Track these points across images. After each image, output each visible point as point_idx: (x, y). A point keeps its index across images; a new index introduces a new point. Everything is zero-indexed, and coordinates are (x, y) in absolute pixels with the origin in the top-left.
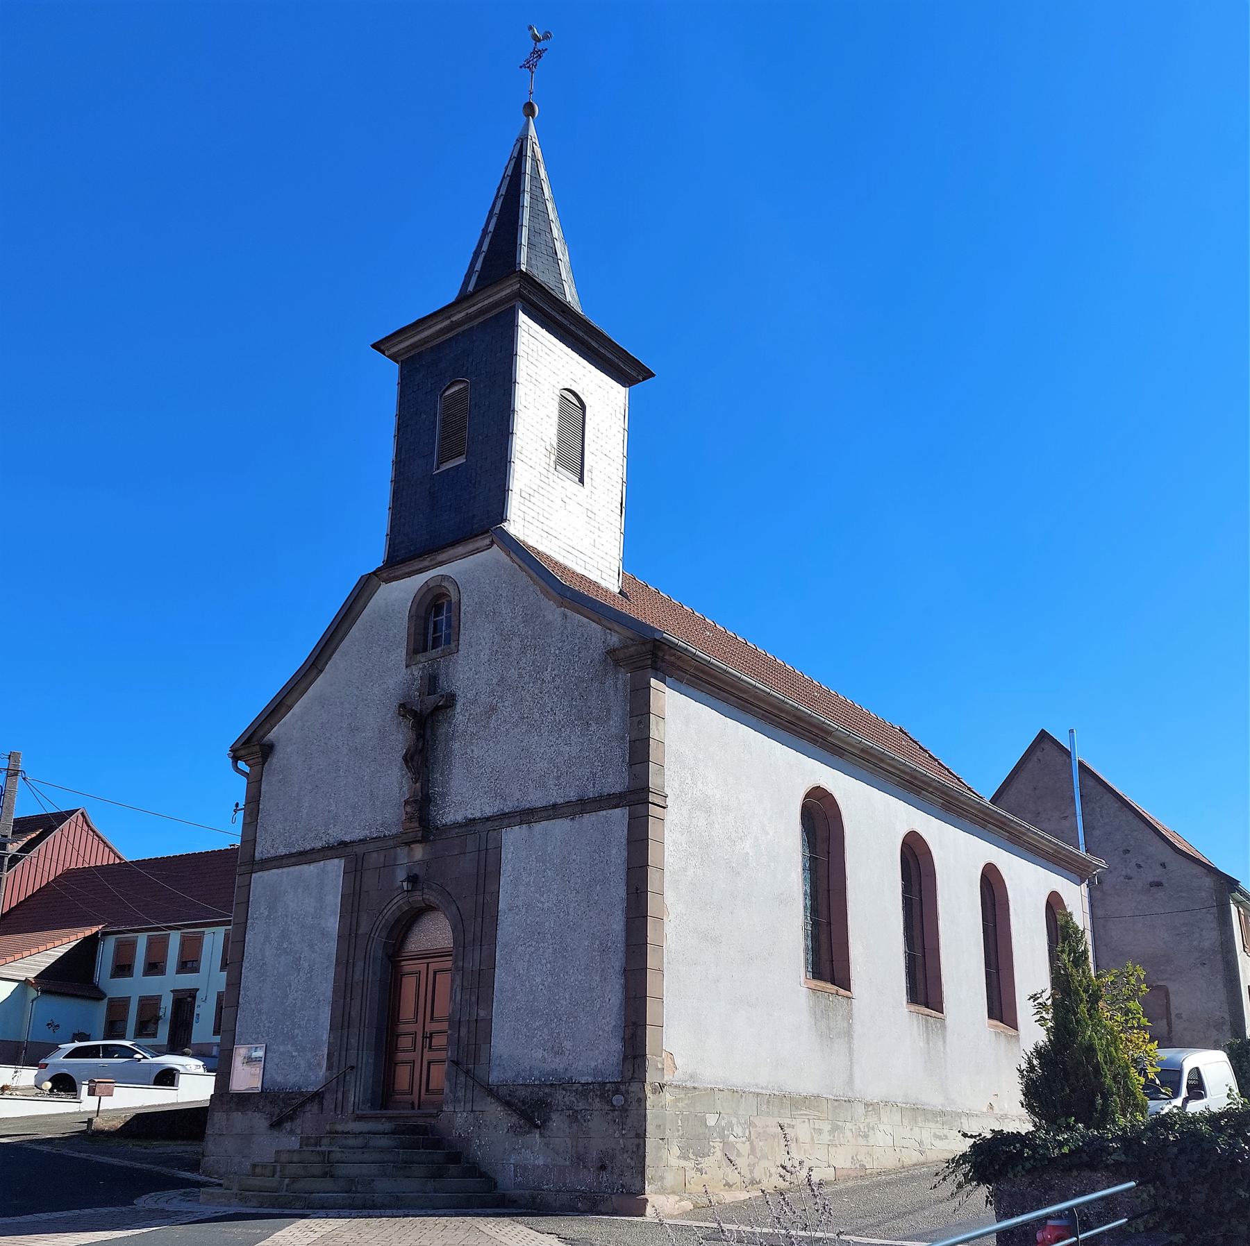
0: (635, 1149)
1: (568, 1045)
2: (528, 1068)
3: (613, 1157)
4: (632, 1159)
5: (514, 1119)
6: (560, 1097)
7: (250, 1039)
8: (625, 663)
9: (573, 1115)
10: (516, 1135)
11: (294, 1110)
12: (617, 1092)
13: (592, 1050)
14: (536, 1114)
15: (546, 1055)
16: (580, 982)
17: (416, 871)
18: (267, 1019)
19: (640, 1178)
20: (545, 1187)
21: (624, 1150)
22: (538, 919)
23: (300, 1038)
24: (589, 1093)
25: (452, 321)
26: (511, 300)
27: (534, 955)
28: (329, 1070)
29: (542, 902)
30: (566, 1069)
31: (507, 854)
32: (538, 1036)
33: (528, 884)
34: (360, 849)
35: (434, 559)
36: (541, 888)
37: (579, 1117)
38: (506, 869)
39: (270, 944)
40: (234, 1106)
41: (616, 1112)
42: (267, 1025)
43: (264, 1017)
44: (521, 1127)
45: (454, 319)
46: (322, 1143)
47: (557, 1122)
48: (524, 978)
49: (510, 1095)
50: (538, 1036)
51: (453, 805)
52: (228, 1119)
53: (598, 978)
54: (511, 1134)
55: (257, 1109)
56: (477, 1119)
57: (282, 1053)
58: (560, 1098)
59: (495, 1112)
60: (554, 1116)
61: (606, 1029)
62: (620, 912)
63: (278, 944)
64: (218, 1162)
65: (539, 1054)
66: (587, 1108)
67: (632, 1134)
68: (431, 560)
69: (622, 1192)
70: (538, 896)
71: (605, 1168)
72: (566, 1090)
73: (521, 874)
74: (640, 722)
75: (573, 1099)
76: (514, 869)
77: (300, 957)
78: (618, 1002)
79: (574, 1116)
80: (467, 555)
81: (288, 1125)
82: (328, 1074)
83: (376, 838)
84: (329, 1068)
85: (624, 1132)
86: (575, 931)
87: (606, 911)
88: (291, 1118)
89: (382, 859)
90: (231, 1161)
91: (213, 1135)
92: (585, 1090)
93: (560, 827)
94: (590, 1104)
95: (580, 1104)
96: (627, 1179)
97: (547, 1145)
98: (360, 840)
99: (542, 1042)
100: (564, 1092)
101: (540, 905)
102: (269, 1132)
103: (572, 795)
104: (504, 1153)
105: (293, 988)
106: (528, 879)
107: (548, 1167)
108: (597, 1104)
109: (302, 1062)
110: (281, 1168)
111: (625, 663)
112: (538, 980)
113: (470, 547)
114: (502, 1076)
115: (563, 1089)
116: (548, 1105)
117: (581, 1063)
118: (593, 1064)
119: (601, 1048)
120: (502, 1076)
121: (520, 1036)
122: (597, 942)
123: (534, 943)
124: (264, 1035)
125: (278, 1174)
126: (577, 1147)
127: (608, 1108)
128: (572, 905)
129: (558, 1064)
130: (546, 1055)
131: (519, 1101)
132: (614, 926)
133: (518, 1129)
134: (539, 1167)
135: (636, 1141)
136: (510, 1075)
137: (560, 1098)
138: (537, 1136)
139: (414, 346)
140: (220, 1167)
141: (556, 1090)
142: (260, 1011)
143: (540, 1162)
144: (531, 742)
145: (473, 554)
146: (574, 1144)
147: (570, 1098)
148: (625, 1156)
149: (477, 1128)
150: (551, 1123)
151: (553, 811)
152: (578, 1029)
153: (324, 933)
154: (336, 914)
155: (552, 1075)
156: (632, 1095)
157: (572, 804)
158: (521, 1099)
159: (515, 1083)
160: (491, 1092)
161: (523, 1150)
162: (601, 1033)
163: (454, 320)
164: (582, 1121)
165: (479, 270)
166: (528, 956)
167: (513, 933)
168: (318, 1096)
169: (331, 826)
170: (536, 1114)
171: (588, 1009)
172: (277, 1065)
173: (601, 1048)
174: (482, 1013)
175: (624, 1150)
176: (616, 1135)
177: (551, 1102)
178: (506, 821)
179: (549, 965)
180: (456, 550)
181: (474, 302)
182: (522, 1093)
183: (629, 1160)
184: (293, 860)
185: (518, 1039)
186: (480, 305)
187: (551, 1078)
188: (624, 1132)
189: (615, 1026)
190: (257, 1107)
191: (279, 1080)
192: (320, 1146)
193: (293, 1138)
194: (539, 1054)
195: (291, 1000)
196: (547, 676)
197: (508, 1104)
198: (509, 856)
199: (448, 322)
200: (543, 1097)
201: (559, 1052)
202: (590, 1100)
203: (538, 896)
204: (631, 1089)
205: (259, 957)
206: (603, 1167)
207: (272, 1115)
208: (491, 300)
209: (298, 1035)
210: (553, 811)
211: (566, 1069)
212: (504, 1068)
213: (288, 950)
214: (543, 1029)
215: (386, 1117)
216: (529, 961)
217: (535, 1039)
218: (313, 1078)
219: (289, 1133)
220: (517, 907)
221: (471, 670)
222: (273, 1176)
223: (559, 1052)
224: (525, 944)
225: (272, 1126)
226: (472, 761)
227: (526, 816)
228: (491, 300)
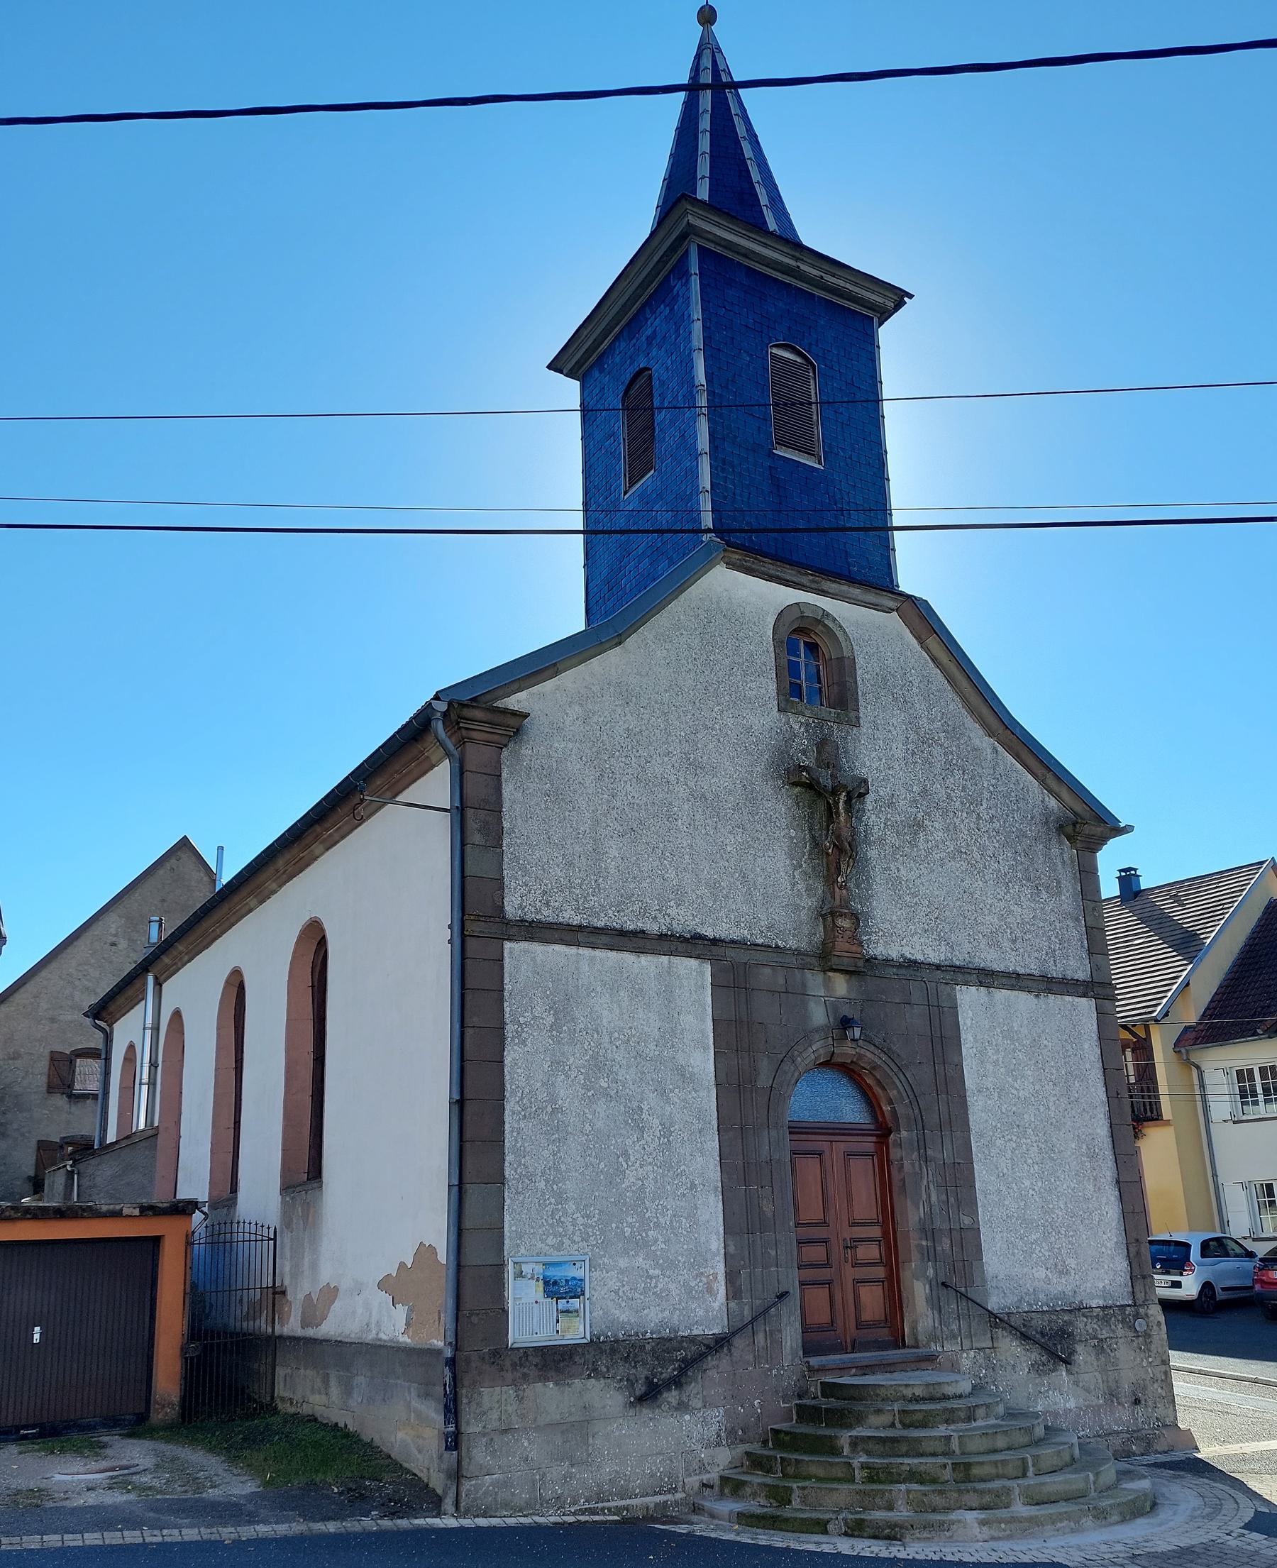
0: (1163, 1378)
1: (1071, 1262)
2: (1031, 1290)
3: (1145, 1388)
4: (1162, 1388)
5: (1035, 1355)
6: (1082, 1325)
7: (540, 1245)
8: (1083, 839)
9: (1099, 1345)
10: (1040, 1375)
11: (683, 1371)
12: (1137, 1316)
13: (1097, 1269)
14: (1059, 1347)
15: (1050, 1274)
16: (1073, 1190)
17: (846, 1011)
18: (578, 1210)
19: (1171, 1408)
20: (1082, 1433)
21: (1154, 1380)
22: (1014, 1109)
23: (663, 1246)
24: (1111, 1318)
25: (798, 267)
26: (874, 310)
27: (1017, 1152)
28: (735, 1297)
29: (1016, 1089)
30: (1075, 1292)
31: (966, 1018)
32: (1037, 1252)
33: (996, 1063)
34: (742, 956)
35: (817, 582)
36: (1012, 1070)
37: (1105, 1346)
38: (967, 1038)
39: (568, 1076)
40: (533, 1372)
41: (1141, 1339)
42: (580, 1221)
43: (571, 1207)
44: (1044, 1365)
45: (803, 267)
46: (978, 1416)
47: (1083, 1355)
48: (1010, 1179)
49: (1024, 1326)
50: (1037, 1252)
51: (881, 933)
52: (520, 1399)
53: (1091, 1187)
54: (1033, 1375)
55: (595, 1373)
56: (988, 1358)
57: (622, 1272)
58: (1081, 1326)
59: (1010, 1348)
60: (1079, 1348)
61: (1108, 1245)
62: (1102, 1116)
63: (587, 1078)
64: (505, 1484)
65: (1041, 1273)
66: (1112, 1335)
67: (1158, 1361)
68: (813, 581)
69: (1158, 1426)
70: (1010, 1080)
71: (1139, 1401)
72: (1086, 1317)
73: (986, 1049)
74: (1094, 909)
75: (1096, 1326)
76: (976, 1040)
77: (640, 1108)
78: (1116, 1215)
79: (1100, 1347)
80: (859, 603)
81: (672, 1396)
82: (732, 1304)
83: (761, 945)
84: (734, 1291)
85: (1150, 1360)
86: (1060, 1130)
87: (1088, 1113)
88: (677, 1382)
89: (781, 981)
90: (544, 1475)
91: (484, 1435)
92: (1106, 1314)
93: (1023, 1001)
94: (1113, 1331)
95: (1104, 1332)
96: (1161, 1411)
97: (1076, 1383)
98: (733, 942)
99: (1043, 1258)
100: (1085, 1319)
101: (1015, 1092)
102: (631, 1412)
103: (1033, 968)
104: (1029, 1399)
105: (632, 1159)
106: (995, 1057)
107: (1081, 1409)
108: (1121, 1331)
109: (672, 1286)
110: (1033, 1460)
111: (1083, 839)
112: (1027, 1183)
113: (871, 597)
114: (1003, 1301)
115: (1084, 1315)
116: (1071, 1335)
117: (1089, 1285)
118: (1101, 1285)
119: (1106, 1267)
120: (1003, 1301)
121: (1016, 1251)
122: (1084, 1147)
123: (1014, 1138)
124: (576, 1238)
125: (1031, 1469)
126: (1108, 1382)
127: (1131, 1334)
128: (1052, 1099)
129: (1062, 1286)
130: (1050, 1274)
131: (1037, 1332)
132: (1099, 1131)
133: (1041, 1368)
134: (1071, 1410)
135: (1163, 1368)
136: (1011, 1300)
137: (1081, 1326)
138: (1064, 1373)
139: (729, 245)
140: (513, 1494)
141: (1076, 1317)
142: (560, 1197)
143: (1071, 1404)
144: (974, 886)
145: (866, 607)
146: (1105, 1378)
147: (1092, 1326)
148: (1156, 1386)
149: (991, 1370)
150: (1076, 1357)
151: (1015, 981)
152: (1080, 1245)
153: (685, 1076)
154: (705, 1048)
155: (1061, 1299)
156: (1152, 1319)
157: (1032, 977)
158: (1039, 1330)
159: (1020, 1310)
160: (997, 1321)
161: (1051, 1393)
162: (1104, 1250)
163: (802, 268)
164: (1109, 1351)
165: (699, 183)
166: (1009, 1152)
167: (987, 1121)
168: (720, 1343)
169: (672, 903)
170: (1059, 1347)
171: (1087, 1221)
172: (616, 1292)
173: (1106, 1267)
174: (967, 1221)
175: (1154, 1380)
176: (1145, 1364)
177: (1073, 1330)
178: (960, 977)
179: (1036, 1167)
180: (851, 589)
181: (837, 273)
182: (1038, 1322)
183: (1160, 1390)
184: (604, 939)
185: (1013, 1254)
186: (842, 283)
187: (1060, 1303)
188: (1150, 1360)
189: (1116, 1243)
190: (595, 1370)
191: (623, 1318)
192: (975, 1420)
193: (687, 1417)
194: (1041, 1273)
195: (632, 1180)
196: (982, 809)
197: (1025, 1337)
198: (969, 1022)
199: (792, 262)
200: (1063, 1325)
201: (1064, 1272)
202: (1113, 1327)
203: (1010, 1080)
204: (1150, 1312)
205: (543, 1096)
206: (1137, 1402)
207: (631, 1383)
208: (857, 290)
209: (656, 1240)
210: (1015, 981)
211: (1075, 1292)
212: (1003, 1291)
213: (612, 1093)
214: (1042, 1242)
215: (856, 1367)
216: (1012, 1159)
217: (1034, 1255)
218: (701, 1313)
219: (676, 1409)
220: (987, 1089)
221: (881, 760)
222: (1024, 1475)
223: (1064, 1272)
224: (1003, 1137)
225: (641, 1400)
226: (900, 883)
227: (987, 978)
228: (857, 290)
